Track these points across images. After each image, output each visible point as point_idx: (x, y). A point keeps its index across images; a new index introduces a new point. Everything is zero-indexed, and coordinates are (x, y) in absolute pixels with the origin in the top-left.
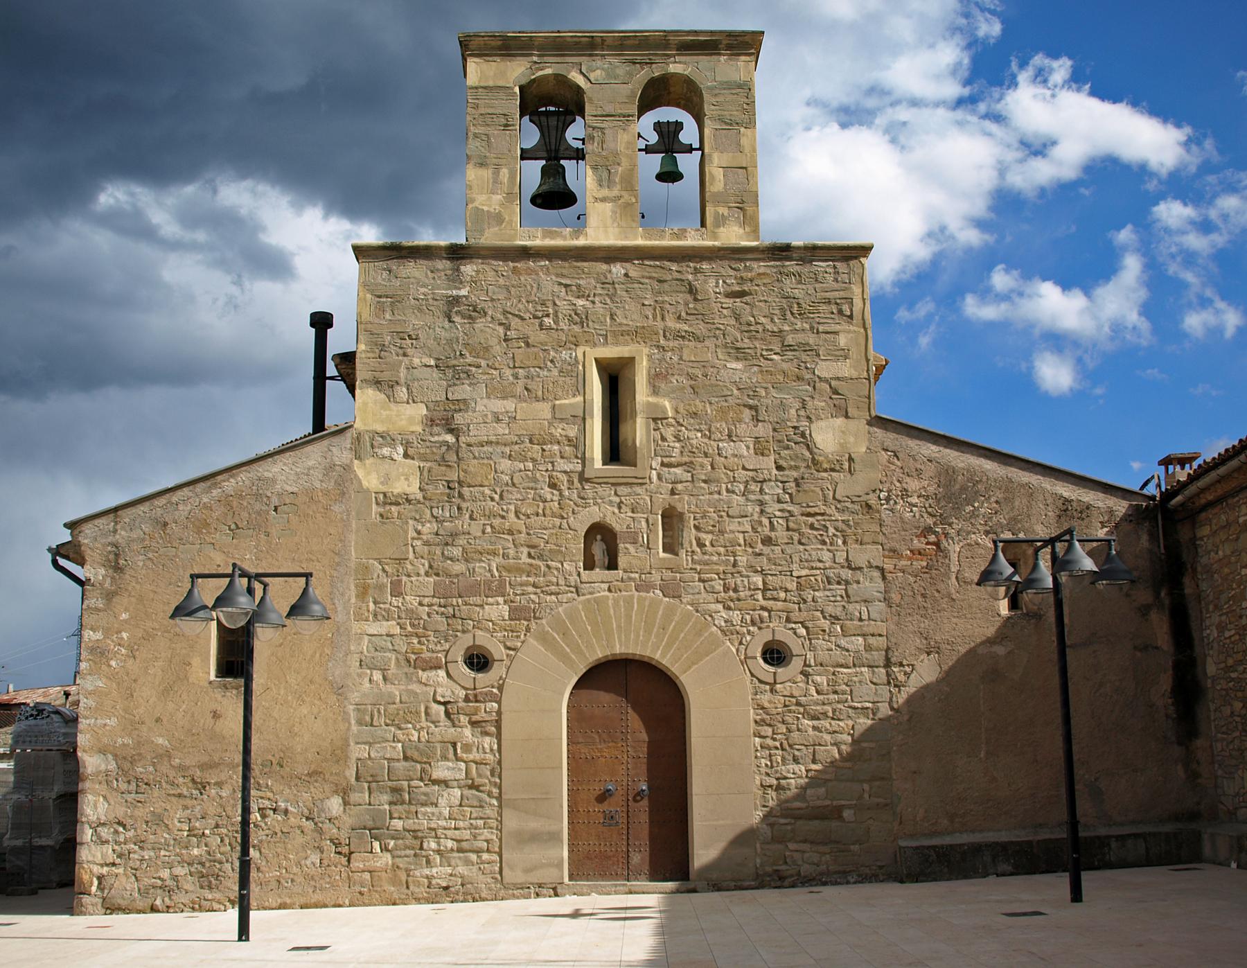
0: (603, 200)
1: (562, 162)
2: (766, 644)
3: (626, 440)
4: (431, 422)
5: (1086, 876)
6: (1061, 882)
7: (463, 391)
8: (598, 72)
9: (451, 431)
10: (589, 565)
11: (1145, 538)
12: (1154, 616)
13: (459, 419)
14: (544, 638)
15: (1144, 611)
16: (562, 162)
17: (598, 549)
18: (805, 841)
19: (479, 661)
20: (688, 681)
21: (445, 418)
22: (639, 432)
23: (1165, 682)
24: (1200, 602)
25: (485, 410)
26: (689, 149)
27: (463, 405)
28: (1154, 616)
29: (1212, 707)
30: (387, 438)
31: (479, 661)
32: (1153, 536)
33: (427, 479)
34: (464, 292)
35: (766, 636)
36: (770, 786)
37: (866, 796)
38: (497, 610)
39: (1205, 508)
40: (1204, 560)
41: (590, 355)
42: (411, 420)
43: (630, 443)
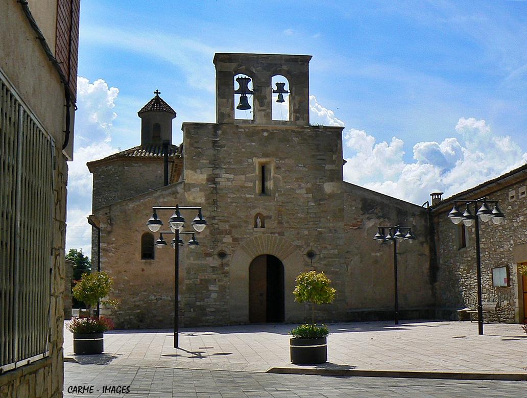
0: (261, 110)
1: (247, 95)
2: (309, 251)
3: (267, 187)
4: (208, 180)
5: (181, 336)
6: (475, 326)
7: (217, 171)
8: (259, 68)
9: (214, 184)
10: (256, 226)
11: (423, 221)
12: (425, 245)
13: (217, 180)
14: (243, 248)
15: (422, 244)
16: (247, 95)
17: (259, 221)
18: (319, 310)
19: (222, 255)
20: (284, 262)
21: (212, 180)
22: (270, 185)
23: (427, 265)
24: (439, 241)
25: (225, 179)
26: (287, 92)
27: (218, 176)
28: (425, 245)
29: (441, 273)
30: (194, 186)
31: (222, 255)
32: (426, 221)
33: (207, 198)
34: (218, 139)
35: (309, 249)
36: (14, 68)
37: (337, 297)
38: (228, 239)
39: (441, 213)
40: (441, 229)
41: (257, 161)
42: (202, 179)
43: (269, 188)
